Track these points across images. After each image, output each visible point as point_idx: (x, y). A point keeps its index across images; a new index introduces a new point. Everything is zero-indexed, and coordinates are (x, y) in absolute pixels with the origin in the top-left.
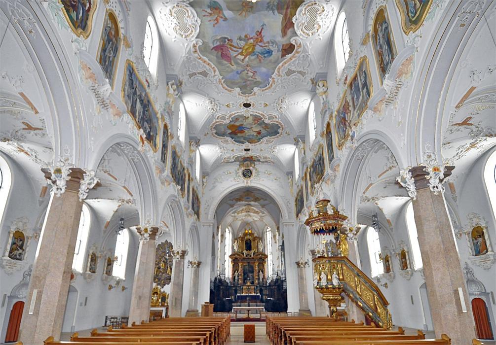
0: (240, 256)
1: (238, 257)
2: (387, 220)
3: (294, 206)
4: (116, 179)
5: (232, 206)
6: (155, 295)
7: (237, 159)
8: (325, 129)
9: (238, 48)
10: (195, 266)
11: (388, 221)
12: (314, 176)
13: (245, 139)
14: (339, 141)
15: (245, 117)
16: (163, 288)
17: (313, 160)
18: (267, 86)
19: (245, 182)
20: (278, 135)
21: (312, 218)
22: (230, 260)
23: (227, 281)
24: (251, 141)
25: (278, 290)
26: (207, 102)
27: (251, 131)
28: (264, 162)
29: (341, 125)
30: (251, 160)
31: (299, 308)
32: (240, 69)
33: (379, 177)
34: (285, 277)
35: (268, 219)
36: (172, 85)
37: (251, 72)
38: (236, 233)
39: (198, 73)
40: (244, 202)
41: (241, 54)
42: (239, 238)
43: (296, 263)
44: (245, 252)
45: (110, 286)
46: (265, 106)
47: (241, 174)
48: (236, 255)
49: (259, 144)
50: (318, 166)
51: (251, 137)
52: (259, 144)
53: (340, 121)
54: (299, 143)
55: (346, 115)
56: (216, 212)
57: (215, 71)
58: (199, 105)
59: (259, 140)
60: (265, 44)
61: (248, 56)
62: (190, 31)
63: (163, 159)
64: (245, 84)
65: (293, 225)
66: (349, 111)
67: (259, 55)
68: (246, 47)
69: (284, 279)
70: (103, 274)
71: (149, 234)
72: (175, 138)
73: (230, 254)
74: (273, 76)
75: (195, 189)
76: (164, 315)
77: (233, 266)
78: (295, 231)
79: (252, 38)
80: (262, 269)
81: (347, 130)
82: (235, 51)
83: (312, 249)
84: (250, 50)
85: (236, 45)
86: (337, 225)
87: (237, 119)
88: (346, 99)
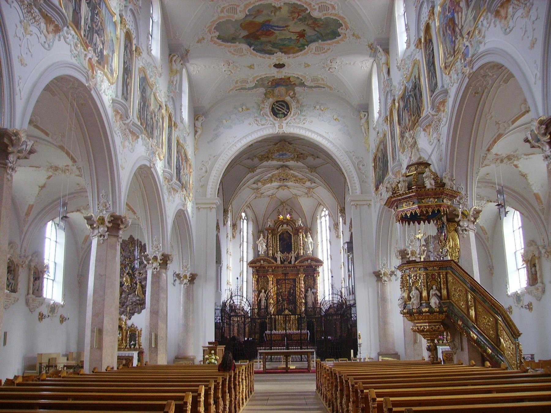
0: (269, 262)
1: (266, 264)
2: (535, 194)
3: (372, 169)
4: (47, 134)
5: (252, 169)
7: (260, 83)
8: (422, 34)
10: (186, 281)
11: (537, 196)
13: (274, 45)
14: (446, 58)
15: (274, 7)
16: (130, 319)
17: (403, 88)
19: (277, 125)
22: (251, 270)
23: (245, 308)
24: (286, 49)
25: (342, 315)
27: (287, 32)
28: (311, 87)
29: (449, 32)
30: (287, 83)
31: (379, 351)
33: (513, 122)
34: (355, 300)
35: (322, 192)
40: (275, 163)
42: (267, 230)
43: (374, 273)
44: (279, 255)
45: (40, 314)
47: (268, 110)
48: (262, 262)
50: (411, 99)
54: (379, 55)
55: (455, 14)
56: (221, 182)
59: (302, 48)
63: (125, 93)
65: (369, 205)
69: (352, 302)
70: (28, 294)
71: (108, 228)
72: (144, 55)
73: (251, 258)
76: (135, 363)
77: (257, 281)
80: (312, 284)
81: (457, 41)
83: (403, 248)
87: (258, 11)
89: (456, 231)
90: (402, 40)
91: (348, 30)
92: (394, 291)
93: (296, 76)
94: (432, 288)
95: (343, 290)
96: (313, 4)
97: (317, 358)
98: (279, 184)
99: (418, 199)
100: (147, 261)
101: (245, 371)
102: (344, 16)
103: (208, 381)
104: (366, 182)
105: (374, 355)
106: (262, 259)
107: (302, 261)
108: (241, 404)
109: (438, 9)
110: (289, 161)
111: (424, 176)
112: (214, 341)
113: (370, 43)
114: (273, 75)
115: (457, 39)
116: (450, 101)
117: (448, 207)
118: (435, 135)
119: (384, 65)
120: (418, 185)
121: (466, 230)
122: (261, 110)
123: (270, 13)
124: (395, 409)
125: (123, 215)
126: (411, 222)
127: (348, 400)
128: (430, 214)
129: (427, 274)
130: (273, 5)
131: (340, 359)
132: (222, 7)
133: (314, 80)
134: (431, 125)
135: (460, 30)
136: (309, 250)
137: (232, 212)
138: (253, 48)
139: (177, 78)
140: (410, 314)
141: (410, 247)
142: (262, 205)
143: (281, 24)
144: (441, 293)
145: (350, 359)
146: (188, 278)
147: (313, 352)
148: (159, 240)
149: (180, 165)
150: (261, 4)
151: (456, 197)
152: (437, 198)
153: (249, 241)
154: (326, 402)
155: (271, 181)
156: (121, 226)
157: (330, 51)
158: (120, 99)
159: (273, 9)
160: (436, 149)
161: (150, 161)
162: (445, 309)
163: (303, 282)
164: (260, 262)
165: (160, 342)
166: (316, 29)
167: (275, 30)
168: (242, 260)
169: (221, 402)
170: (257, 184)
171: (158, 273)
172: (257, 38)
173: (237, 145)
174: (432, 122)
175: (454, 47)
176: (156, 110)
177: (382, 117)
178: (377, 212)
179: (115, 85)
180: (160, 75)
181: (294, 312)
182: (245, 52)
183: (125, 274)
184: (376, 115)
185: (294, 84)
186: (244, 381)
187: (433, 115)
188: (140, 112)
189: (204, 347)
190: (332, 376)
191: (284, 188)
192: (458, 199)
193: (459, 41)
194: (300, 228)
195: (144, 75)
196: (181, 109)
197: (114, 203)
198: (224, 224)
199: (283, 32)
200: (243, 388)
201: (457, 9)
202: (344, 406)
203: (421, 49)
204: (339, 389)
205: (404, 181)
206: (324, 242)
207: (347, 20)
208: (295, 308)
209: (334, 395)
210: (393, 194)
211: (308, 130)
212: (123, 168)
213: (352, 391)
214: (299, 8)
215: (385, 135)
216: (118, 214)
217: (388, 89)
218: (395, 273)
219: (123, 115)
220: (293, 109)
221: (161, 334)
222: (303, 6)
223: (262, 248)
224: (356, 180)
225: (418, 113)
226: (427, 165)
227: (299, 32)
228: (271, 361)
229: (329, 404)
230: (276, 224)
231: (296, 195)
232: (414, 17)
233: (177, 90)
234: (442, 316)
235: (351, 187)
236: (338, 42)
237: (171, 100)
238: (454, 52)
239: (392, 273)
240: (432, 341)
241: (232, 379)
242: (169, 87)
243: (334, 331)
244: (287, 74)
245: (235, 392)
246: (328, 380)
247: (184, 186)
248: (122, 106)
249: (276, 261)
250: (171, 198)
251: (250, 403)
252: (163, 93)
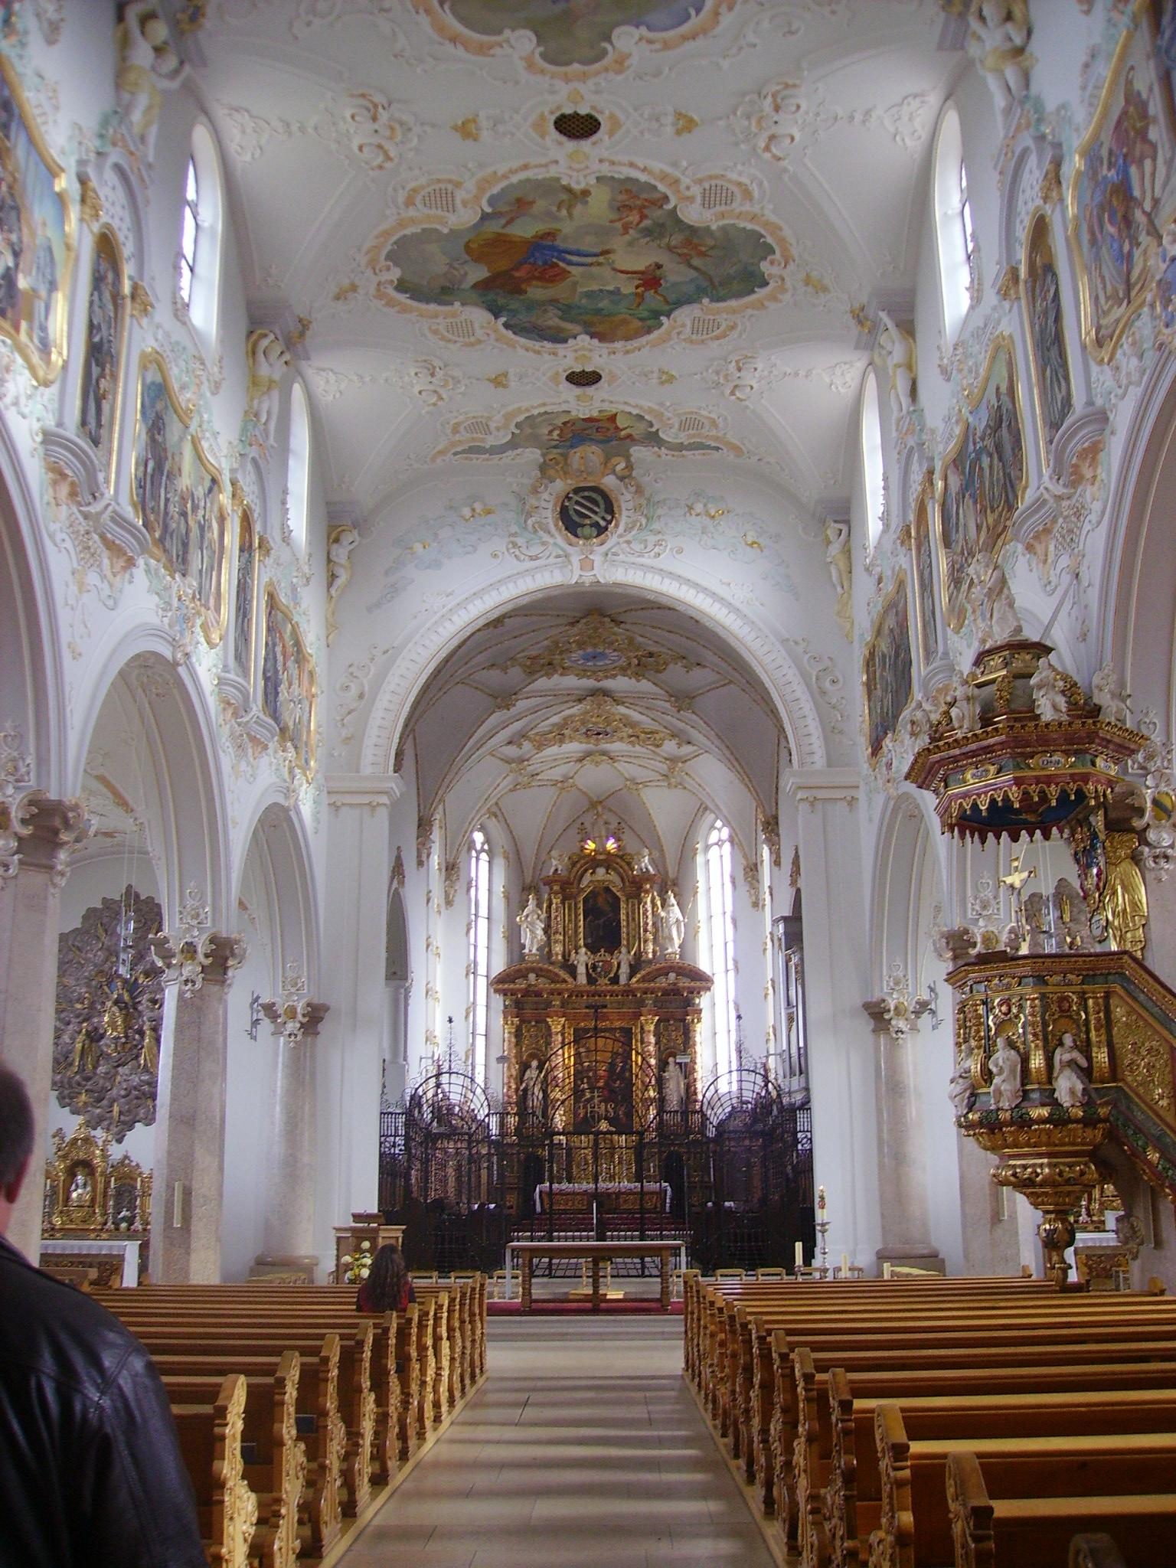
0: (554, 979)
1: (543, 984)
5: (504, 699)
6: (80, 1179)
7: (526, 431)
8: (1022, 255)
10: (292, 1026)
12: (968, 517)
13: (567, 312)
15: (568, 190)
16: (120, 1141)
17: (958, 430)
18: (688, 17)
19: (575, 560)
20: (761, 293)
21: (949, 746)
22: (499, 1001)
24: (603, 326)
25: (774, 1130)
26: (348, 114)
27: (606, 272)
28: (680, 447)
29: (1111, 229)
30: (603, 431)
31: (879, 1246)
34: (807, 1089)
35: (712, 772)
36: (146, 19)
38: (529, 854)
40: (571, 681)
42: (549, 882)
43: (867, 1006)
44: (582, 959)
46: (678, 133)
47: (549, 515)
48: (532, 976)
50: (985, 461)
51: (604, 304)
53: (1101, 208)
54: (883, 339)
55: (1133, 171)
58: (302, 129)
59: (652, 321)
65: (852, 802)
66: (1147, 148)
69: (798, 1098)
71: (20, 839)
72: (162, 313)
73: (499, 966)
75: (283, 599)
76: (130, 1278)
77: (518, 1034)
78: (866, 825)
83: (957, 924)
86: (1085, 778)
87: (518, 203)
88: (1129, 83)
89: (1136, 859)
90: (955, 293)
91: (792, 267)
92: (933, 1061)
93: (635, 412)
94: (1061, 1044)
95: (772, 1062)
96: (686, 181)
97: (689, 1265)
98: (584, 747)
99: (1013, 756)
100: (163, 958)
101: (462, 1305)
102: (781, 223)
103: (277, 1351)
104: (841, 732)
105: (865, 1259)
106: (532, 970)
107: (651, 978)
108: (428, 1423)
109: (1075, 163)
110: (614, 676)
111: (1033, 681)
112: (376, 1211)
113: (857, 306)
114: (565, 407)
115: (1138, 244)
117: (1111, 783)
118: (1064, 561)
119: (899, 371)
120: (1013, 712)
121: (1166, 857)
122: (529, 515)
123: (554, 209)
124: (1004, 1508)
125: (69, 799)
126: (990, 835)
127: (791, 1425)
128: (1054, 803)
129: (1043, 997)
130: (564, 182)
131: (761, 1271)
133: (690, 423)
134: (1053, 530)
135: (1148, 215)
136: (672, 945)
137: (444, 827)
138: (503, 319)
139: (270, 404)
140: (986, 1127)
141: (981, 923)
142: (535, 811)
143: (588, 243)
144: (1089, 1058)
145: (791, 1271)
146: (300, 1017)
147: (678, 1248)
148: (203, 893)
149: (276, 671)
150: (528, 180)
151: (1133, 752)
152: (1076, 753)
153: (494, 916)
154: (714, 1417)
155: (561, 738)
156: (64, 837)
157: (735, 334)
158: (71, 429)
159: (564, 196)
160: (1067, 605)
161: (174, 644)
162: (1103, 1111)
163: (652, 1040)
164: (525, 977)
165: (198, 1211)
166: (696, 262)
167: (570, 263)
168: (472, 970)
169: (336, 1429)
170: (520, 746)
171: (198, 994)
172: (516, 289)
173: (455, 618)
174: (1054, 521)
175: (1129, 273)
176: (200, 492)
177: (893, 527)
178: (877, 818)
179: (54, 389)
180: (216, 389)
181: (622, 1126)
182: (479, 333)
183: (109, 1004)
184: (874, 527)
185: (629, 436)
186: (445, 1345)
187: (1059, 498)
188: (141, 486)
189: (338, 1230)
190: (733, 1332)
191: (599, 758)
192: (1140, 757)
193: (1145, 252)
194: (646, 877)
195: (159, 379)
196: (284, 503)
197: (42, 761)
198: (420, 863)
199: (595, 270)
200: (440, 1367)
201: (1137, 153)
202: (776, 1446)
203: (1018, 298)
204: (757, 1380)
205: (968, 699)
206: (714, 922)
207: (787, 233)
208: (629, 1115)
209: (740, 1399)
210: (933, 740)
211: (670, 574)
212: (77, 655)
213: (807, 1400)
214: (645, 196)
215: (901, 585)
216: (53, 796)
217: (911, 442)
218: (933, 1006)
219: (80, 484)
220: (624, 513)
221: (202, 1186)
222: (655, 187)
223: (532, 938)
224: (813, 727)
225: (1007, 500)
226: (1042, 649)
227: (641, 273)
228: (550, 1276)
229: (724, 1426)
230: (574, 864)
231: (632, 780)
232: (995, 204)
233: (271, 441)
234: (1097, 1134)
235: (799, 746)
236: (760, 305)
237: (250, 467)
238: (1129, 287)
239: (923, 1007)
240: (1061, 1214)
241: (392, 1341)
242: (244, 430)
243: (741, 1189)
244: (606, 406)
245: (405, 1383)
246: (722, 1344)
247: (288, 735)
248: (74, 454)
249: (574, 975)
250: (243, 766)
251: (469, 1415)
252: (223, 440)
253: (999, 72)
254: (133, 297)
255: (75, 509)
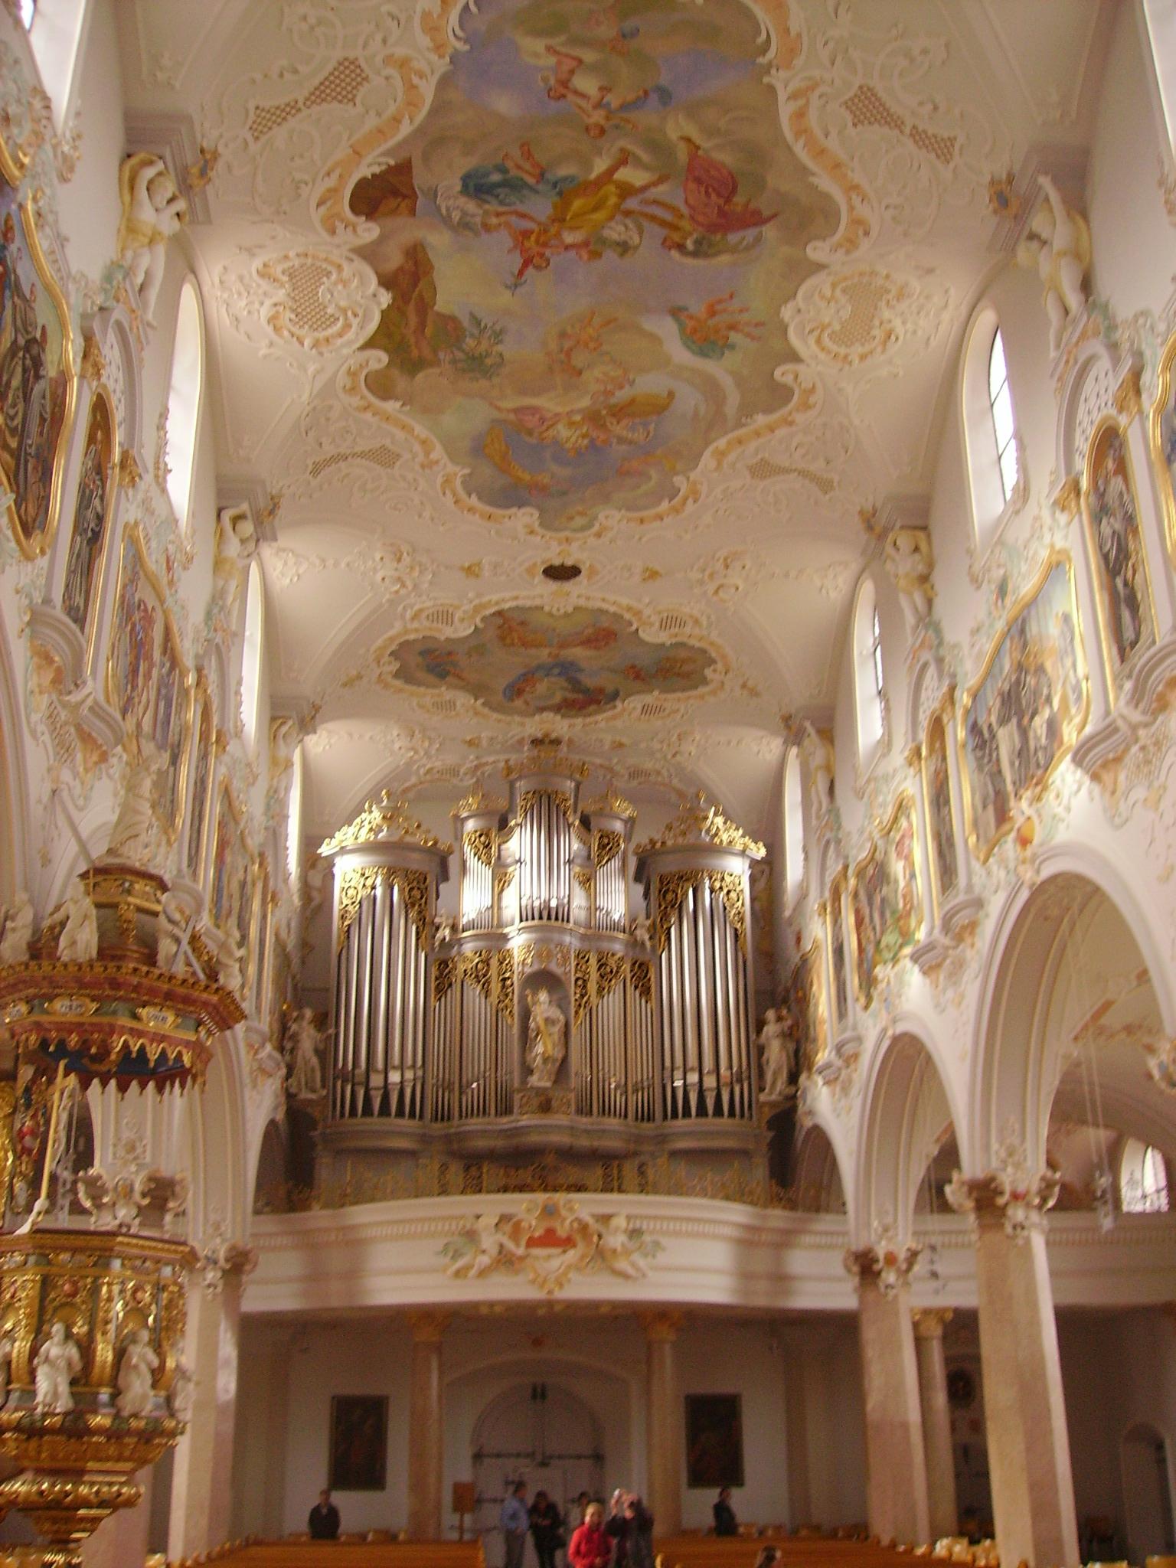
9: (645, 215)
20: (702, 690)
32: (647, 117)
36: (236, 520)
37: (583, 96)
39: (897, 124)
41: (626, 191)
49: (608, 720)
52: (608, 720)
57: (800, 115)
60: (508, 225)
61: (593, 176)
62: (340, 324)
64: (629, 24)
67: (531, 181)
68: (599, 216)
71: (139, 1208)
74: (443, 65)
79: (567, 248)
82: (656, 202)
83: (980, 1174)
84: (577, 204)
85: (646, 224)
91: (730, 675)
96: (647, 612)
116: (988, 927)
132: (416, 608)
253: (909, 594)
254: (123, 465)
255: (54, 697)
